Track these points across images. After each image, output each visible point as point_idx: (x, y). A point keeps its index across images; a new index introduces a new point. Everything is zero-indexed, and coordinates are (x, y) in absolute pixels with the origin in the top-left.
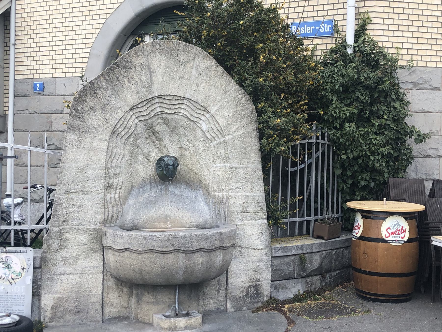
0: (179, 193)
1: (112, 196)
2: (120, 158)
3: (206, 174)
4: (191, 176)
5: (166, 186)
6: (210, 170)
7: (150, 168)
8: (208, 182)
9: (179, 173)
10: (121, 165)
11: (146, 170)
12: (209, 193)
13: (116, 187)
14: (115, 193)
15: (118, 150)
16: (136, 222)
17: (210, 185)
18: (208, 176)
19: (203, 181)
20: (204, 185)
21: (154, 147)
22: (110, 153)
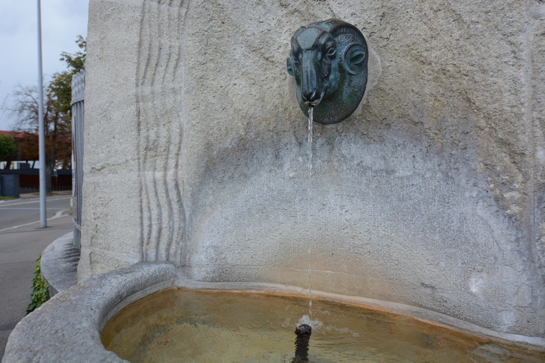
0: (380, 164)
1: (159, 175)
2: (172, 64)
3: (492, 62)
4: (427, 90)
5: (330, 143)
6: (521, 38)
7: (275, 85)
8: (508, 98)
9: (377, 88)
10: (177, 86)
11: (260, 86)
12: (517, 156)
13: (167, 150)
14: (165, 169)
15: (165, 41)
16: (231, 258)
17: (519, 116)
18: (509, 71)
19: (478, 99)
20: (488, 118)
21: (282, 12)
22: (145, 53)
